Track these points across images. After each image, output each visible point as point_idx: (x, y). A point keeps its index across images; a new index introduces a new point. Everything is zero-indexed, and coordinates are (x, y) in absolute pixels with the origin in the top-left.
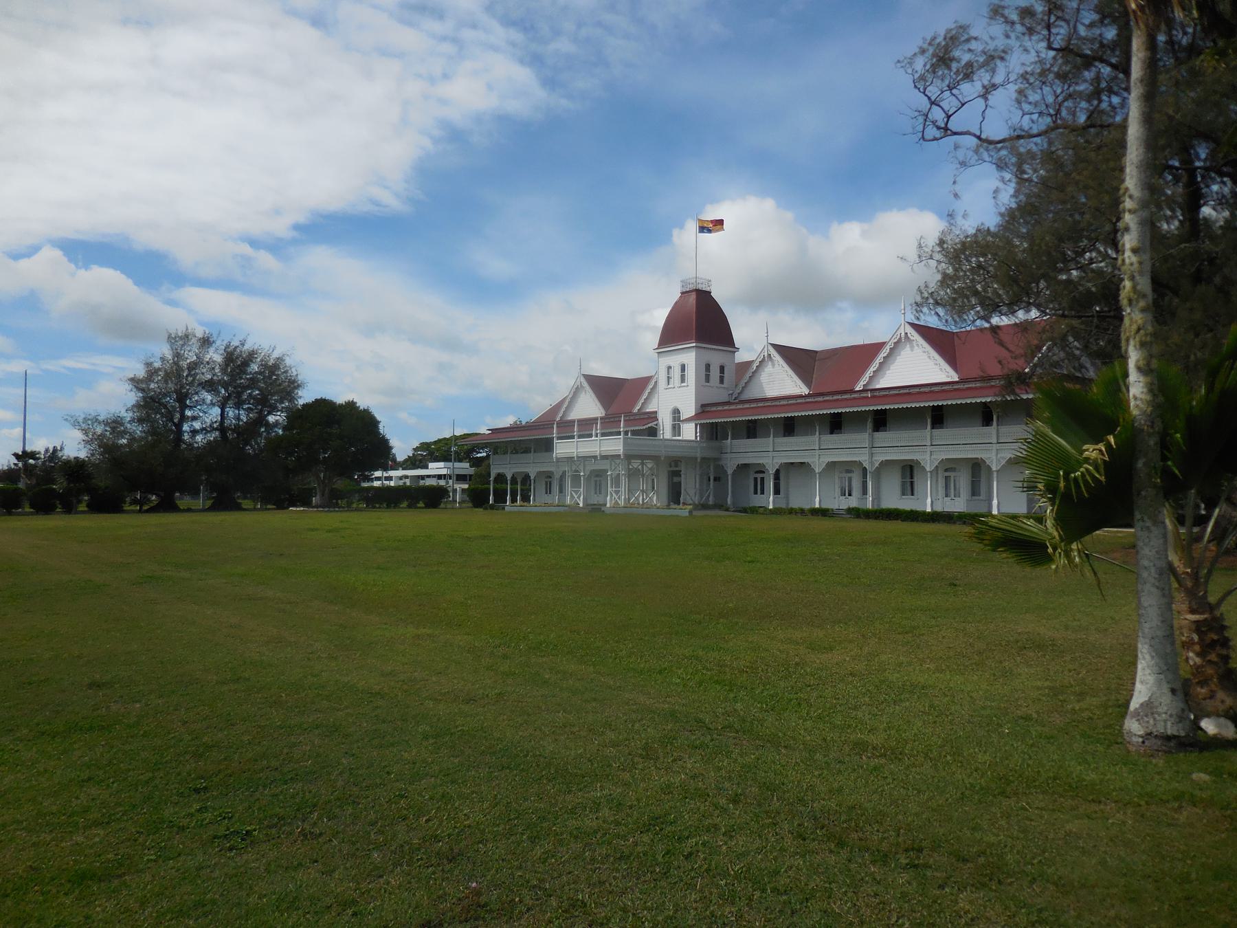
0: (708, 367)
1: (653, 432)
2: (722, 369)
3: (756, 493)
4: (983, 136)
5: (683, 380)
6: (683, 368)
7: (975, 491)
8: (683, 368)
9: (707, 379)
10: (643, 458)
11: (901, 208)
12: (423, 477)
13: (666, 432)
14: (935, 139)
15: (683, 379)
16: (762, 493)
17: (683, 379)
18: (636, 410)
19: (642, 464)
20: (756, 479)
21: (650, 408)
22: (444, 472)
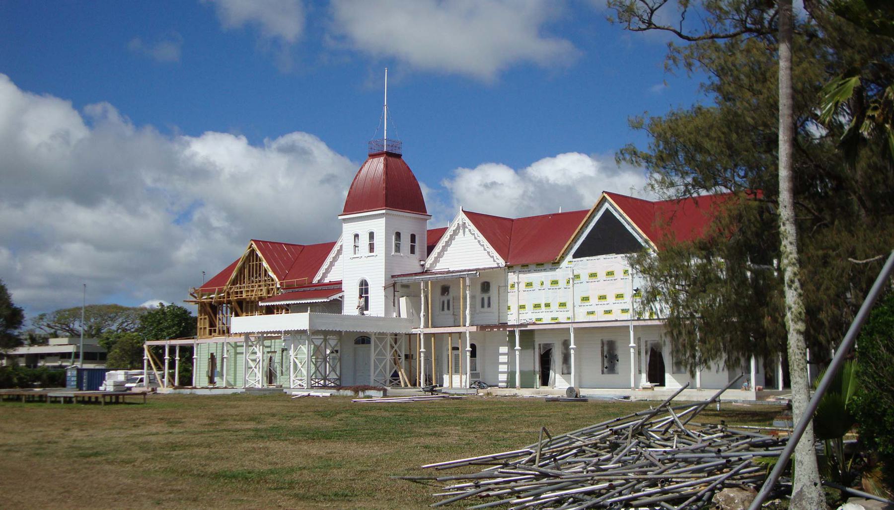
0: (398, 235)
1: (336, 306)
2: (413, 237)
3: (483, 306)
4: (683, 33)
5: (372, 249)
6: (371, 235)
7: (769, 382)
8: (371, 235)
9: (398, 249)
10: (326, 333)
11: (218, 135)
12: (43, 356)
13: (351, 307)
14: (640, 29)
15: (372, 248)
16: (489, 305)
17: (372, 248)
18: (315, 281)
19: (325, 340)
20: (483, 299)
21: (331, 278)
22: (71, 349)
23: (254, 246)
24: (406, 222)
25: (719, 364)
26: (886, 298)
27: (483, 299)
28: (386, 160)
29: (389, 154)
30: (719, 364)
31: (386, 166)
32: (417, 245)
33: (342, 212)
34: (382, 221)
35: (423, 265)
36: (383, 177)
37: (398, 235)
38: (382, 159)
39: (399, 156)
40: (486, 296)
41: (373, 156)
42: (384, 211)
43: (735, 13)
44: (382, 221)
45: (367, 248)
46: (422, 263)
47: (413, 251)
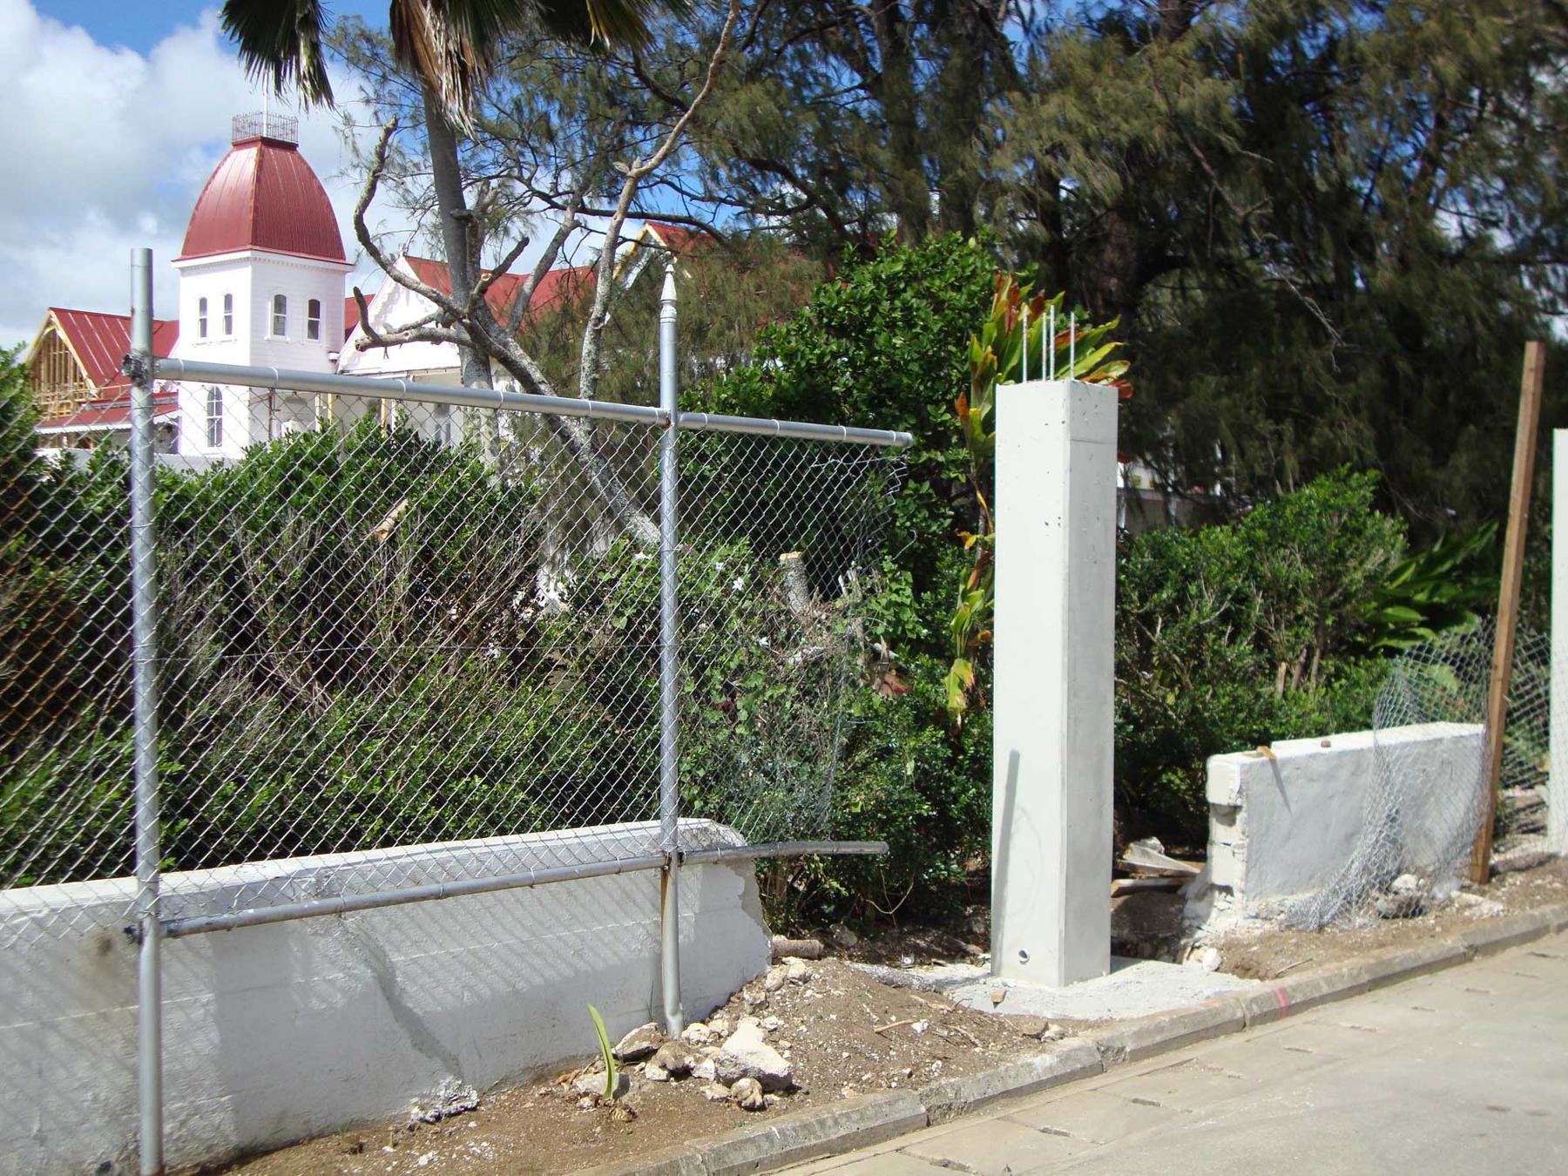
0: (280, 303)
2: (314, 307)
6: (228, 300)
8: (228, 300)
9: (279, 327)
23: (55, 319)
24: (298, 275)
25: (1476, 554)
26: (926, 809)
27: (438, 426)
28: (261, 154)
29: (268, 143)
30: (1476, 554)
31: (260, 165)
32: (323, 321)
33: (179, 255)
34: (246, 273)
35: (334, 361)
36: (251, 188)
37: (280, 303)
38: (252, 152)
39: (292, 147)
40: (441, 421)
41: (239, 145)
42: (248, 254)
43: (1387, 71)
44: (246, 273)
45: (222, 324)
46: (333, 356)
47: (313, 329)
